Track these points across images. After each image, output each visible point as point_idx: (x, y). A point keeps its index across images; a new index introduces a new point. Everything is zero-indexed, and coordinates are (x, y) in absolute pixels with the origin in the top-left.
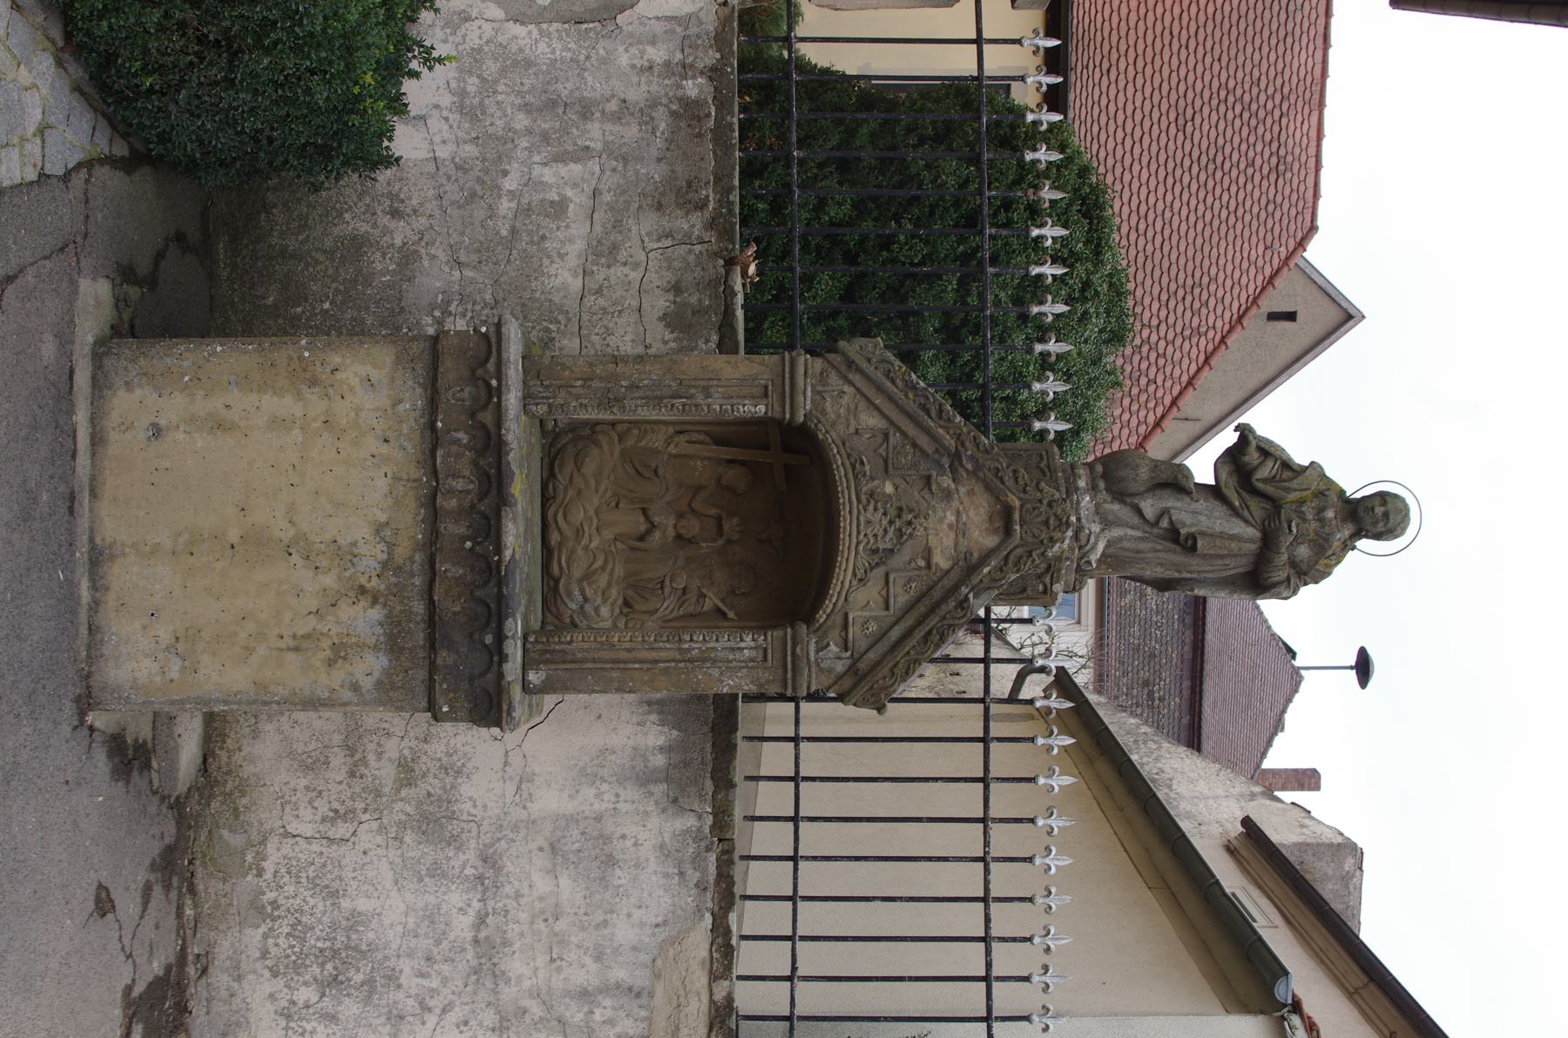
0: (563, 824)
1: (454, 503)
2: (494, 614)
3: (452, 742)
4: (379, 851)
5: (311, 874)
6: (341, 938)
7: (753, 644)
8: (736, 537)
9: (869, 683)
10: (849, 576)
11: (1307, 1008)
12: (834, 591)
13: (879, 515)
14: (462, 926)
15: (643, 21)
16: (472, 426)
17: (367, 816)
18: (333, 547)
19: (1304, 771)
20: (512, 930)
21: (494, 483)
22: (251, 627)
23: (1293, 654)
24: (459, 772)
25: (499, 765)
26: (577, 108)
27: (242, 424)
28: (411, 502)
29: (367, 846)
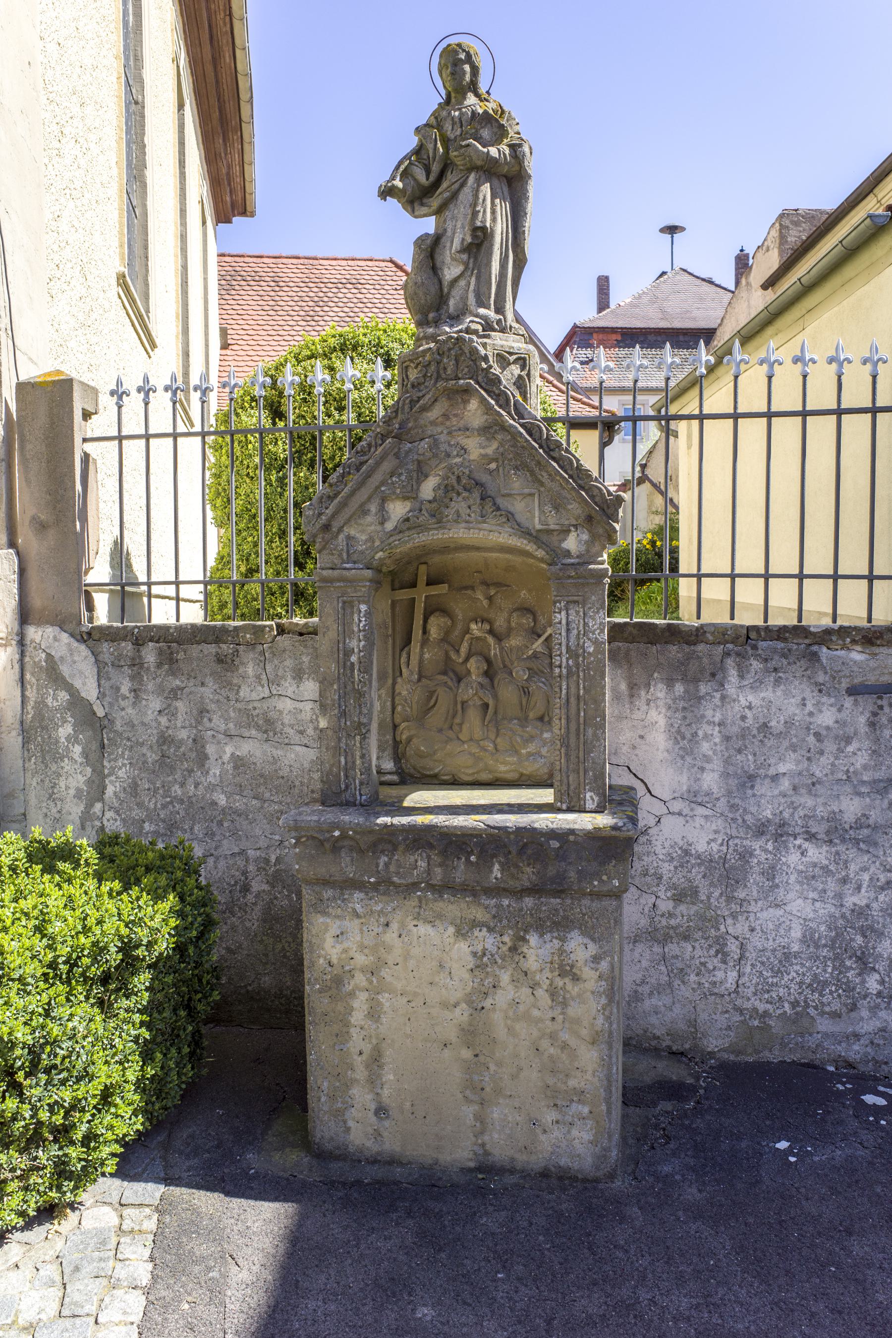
0: (731, 768)
1: (438, 870)
3: (661, 857)
4: (752, 918)
5: (769, 974)
6: (825, 952)
7: (563, 613)
14: (816, 854)
15: (101, 696)
17: (722, 927)
18: (476, 973)
19: (737, 264)
20: (820, 811)
22: (545, 1044)
24: (687, 852)
25: (681, 820)
26: (165, 748)
27: (374, 1041)
28: (440, 905)
29: (746, 929)
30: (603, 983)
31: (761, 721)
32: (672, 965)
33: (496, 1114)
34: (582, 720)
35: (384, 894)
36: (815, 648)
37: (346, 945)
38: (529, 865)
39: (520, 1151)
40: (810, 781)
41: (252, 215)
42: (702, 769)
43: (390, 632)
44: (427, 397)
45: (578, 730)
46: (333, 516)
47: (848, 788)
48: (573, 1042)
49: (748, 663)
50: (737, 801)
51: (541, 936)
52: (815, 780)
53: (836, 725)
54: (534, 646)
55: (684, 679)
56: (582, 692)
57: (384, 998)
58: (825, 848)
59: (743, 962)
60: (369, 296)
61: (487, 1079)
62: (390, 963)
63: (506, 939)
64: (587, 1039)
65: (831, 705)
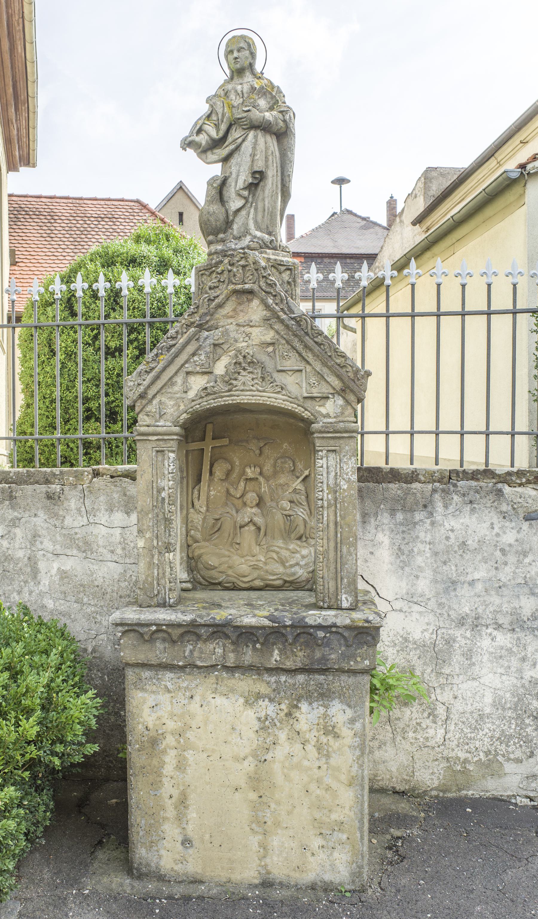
1: (232, 655)
2: (304, 633)
3: (387, 643)
4: (455, 688)
5: (469, 731)
6: (509, 713)
7: (325, 459)
8: (258, 470)
9: (352, 385)
10: (280, 396)
11: (523, 160)
12: (289, 406)
13: (240, 377)
14: (503, 639)
16: (182, 642)
17: (433, 696)
20: (506, 607)
21: (219, 630)
23: (334, 214)
24: (406, 640)
25: (402, 615)
26: (6, 564)
27: (181, 788)
28: (232, 682)
30: (358, 739)
31: (461, 540)
32: (395, 725)
33: (275, 842)
34: (339, 539)
35: (189, 674)
36: (500, 486)
37: (159, 713)
38: (301, 650)
39: (294, 870)
40: (497, 585)
41: (34, 166)
42: (417, 577)
43: (185, 474)
44: (221, 297)
45: (336, 548)
46: (149, 387)
47: (526, 590)
48: (335, 785)
49: (450, 497)
50: (443, 600)
51: (310, 704)
52: (501, 584)
53: (516, 543)
54: (294, 485)
55: (404, 509)
56: (338, 519)
57: (189, 755)
58: (509, 635)
59: (448, 722)
60: (121, 227)
61: (268, 815)
62: (194, 727)
63: (283, 706)
64: (346, 782)
65: (512, 528)
